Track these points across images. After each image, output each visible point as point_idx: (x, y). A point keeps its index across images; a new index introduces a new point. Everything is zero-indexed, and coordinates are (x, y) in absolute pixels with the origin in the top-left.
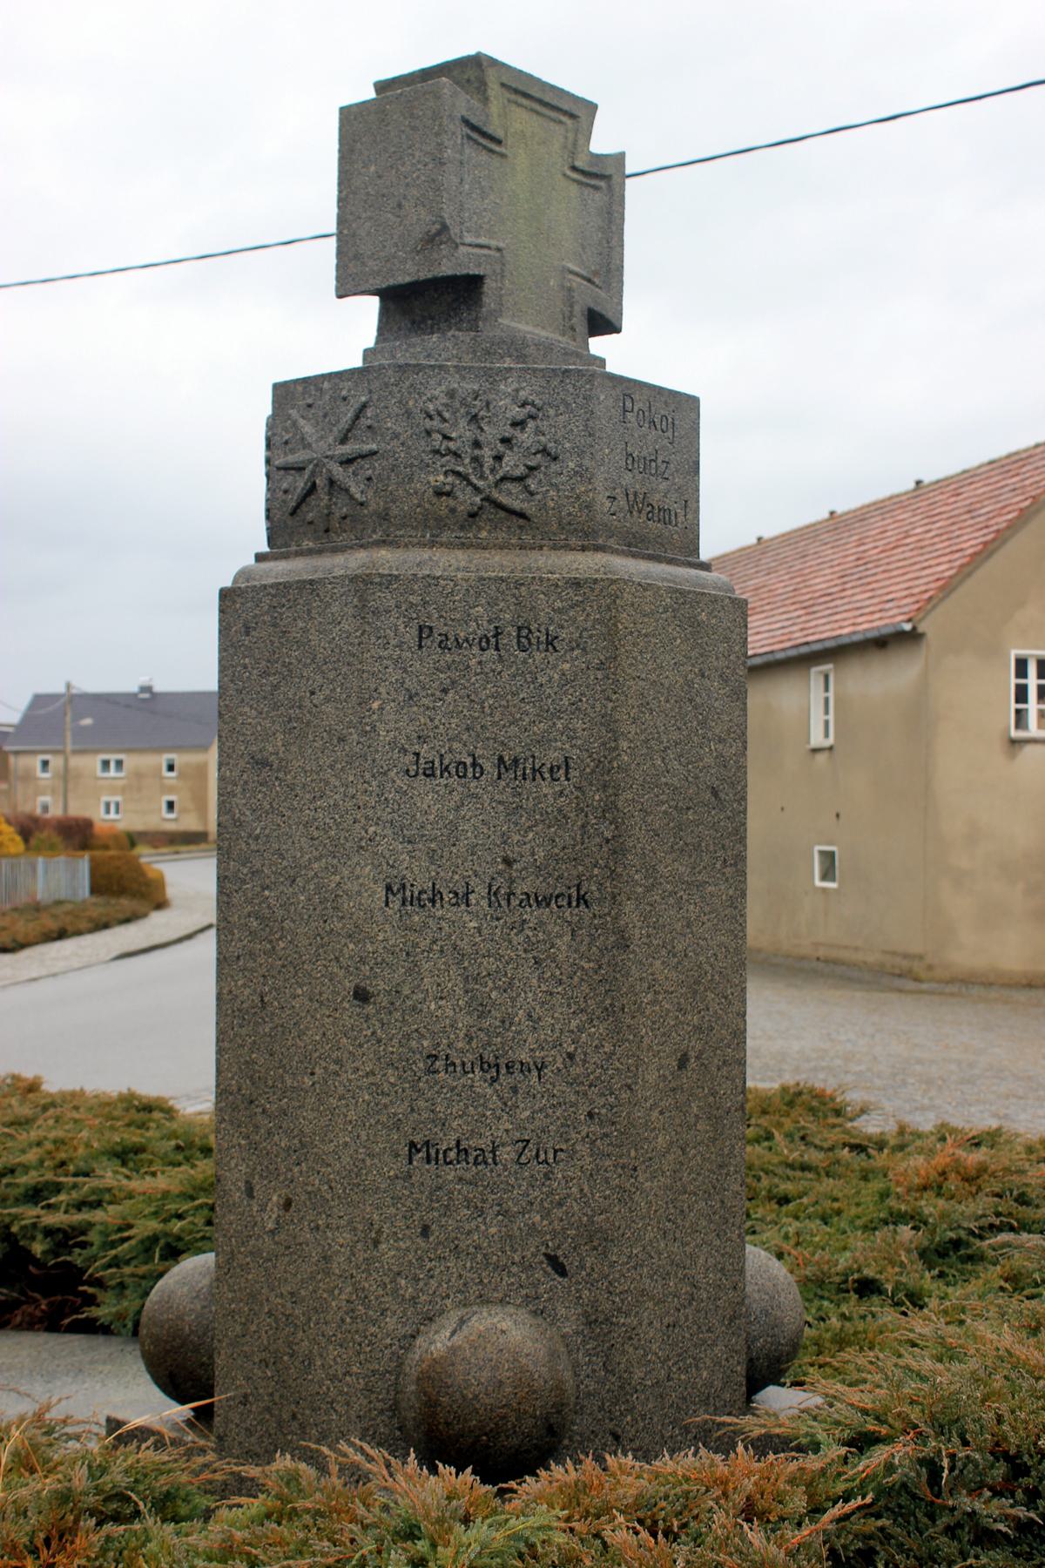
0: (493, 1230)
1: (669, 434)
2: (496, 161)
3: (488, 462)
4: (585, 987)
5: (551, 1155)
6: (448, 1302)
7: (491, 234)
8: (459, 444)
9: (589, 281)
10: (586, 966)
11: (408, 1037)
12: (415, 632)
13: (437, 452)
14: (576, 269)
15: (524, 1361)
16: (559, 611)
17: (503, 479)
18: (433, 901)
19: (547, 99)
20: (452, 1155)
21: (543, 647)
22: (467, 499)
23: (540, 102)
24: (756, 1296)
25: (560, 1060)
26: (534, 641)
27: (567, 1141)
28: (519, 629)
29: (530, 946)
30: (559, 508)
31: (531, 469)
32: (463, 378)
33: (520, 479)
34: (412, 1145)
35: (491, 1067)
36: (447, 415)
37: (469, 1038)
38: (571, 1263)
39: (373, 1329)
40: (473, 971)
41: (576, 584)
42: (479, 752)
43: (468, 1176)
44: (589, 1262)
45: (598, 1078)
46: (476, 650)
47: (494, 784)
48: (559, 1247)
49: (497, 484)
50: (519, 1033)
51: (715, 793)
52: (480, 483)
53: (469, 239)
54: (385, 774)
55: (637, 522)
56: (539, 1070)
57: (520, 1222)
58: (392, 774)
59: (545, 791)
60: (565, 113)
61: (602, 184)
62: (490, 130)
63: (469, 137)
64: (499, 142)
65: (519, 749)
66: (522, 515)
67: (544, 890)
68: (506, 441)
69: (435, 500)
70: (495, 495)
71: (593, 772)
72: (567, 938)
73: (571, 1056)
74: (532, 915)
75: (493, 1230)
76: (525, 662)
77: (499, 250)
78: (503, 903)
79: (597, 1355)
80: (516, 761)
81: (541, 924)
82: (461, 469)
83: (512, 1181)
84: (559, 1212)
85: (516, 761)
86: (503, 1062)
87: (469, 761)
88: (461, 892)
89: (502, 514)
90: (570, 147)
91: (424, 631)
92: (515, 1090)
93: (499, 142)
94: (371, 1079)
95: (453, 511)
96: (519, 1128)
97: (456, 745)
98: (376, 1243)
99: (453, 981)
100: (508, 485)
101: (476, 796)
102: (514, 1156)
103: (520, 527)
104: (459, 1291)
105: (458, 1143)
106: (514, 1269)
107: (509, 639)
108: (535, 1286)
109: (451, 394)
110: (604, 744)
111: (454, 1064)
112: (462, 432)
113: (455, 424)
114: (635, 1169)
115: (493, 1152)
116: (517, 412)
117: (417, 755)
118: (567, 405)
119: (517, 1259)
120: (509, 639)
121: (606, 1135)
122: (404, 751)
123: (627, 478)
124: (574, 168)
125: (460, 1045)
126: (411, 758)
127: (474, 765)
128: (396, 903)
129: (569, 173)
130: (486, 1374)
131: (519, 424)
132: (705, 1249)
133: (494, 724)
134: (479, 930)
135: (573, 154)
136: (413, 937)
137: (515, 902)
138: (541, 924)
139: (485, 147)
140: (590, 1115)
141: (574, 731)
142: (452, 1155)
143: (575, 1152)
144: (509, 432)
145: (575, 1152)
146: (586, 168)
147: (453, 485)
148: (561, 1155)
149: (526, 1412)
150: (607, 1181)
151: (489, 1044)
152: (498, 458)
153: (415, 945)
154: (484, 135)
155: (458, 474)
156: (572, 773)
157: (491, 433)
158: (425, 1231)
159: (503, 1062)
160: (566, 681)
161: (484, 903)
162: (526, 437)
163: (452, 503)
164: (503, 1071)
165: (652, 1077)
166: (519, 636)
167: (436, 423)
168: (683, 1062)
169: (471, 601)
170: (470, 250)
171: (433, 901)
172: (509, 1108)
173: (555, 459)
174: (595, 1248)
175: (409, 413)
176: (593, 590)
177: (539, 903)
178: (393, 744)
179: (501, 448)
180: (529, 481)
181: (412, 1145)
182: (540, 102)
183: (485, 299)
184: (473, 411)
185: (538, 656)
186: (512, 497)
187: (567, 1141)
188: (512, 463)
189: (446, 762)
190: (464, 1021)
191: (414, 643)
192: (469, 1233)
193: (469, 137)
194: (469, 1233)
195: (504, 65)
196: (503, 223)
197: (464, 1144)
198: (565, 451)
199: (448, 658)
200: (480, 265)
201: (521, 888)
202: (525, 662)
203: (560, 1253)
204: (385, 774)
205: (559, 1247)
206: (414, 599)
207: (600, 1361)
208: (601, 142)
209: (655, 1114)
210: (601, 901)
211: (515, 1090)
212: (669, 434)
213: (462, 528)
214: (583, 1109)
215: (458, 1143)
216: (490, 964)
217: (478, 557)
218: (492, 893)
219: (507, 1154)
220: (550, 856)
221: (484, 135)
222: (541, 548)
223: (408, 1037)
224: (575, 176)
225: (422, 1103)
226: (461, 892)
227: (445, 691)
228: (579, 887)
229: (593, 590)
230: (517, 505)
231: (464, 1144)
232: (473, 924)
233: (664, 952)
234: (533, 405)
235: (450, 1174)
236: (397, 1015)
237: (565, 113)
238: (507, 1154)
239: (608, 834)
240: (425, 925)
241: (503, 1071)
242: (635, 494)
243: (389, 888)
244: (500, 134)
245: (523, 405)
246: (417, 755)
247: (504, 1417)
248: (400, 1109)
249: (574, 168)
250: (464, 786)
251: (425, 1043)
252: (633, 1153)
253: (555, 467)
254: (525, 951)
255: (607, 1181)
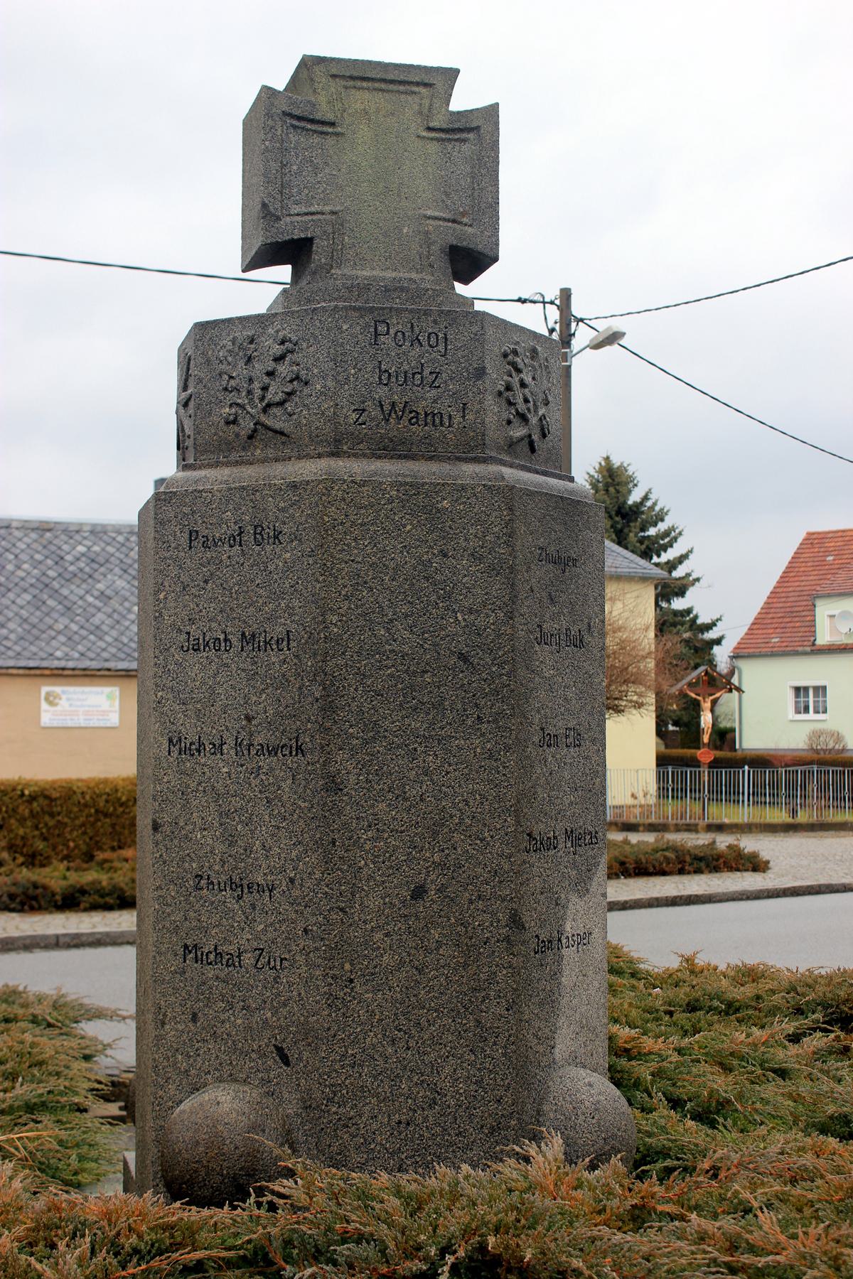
0: (239, 1021)
1: (441, 348)
2: (331, 141)
3: (258, 392)
4: (301, 823)
5: (278, 963)
6: (209, 1077)
7: (326, 201)
8: (237, 381)
9: (454, 221)
10: (303, 805)
11: (183, 860)
12: (187, 536)
13: (226, 389)
14: (437, 214)
15: (220, 1128)
16: (283, 510)
17: (269, 405)
18: (199, 751)
19: (390, 77)
20: (212, 957)
21: (271, 541)
22: (247, 425)
23: (384, 81)
24: (552, 1115)
25: (284, 883)
26: (265, 536)
27: (290, 951)
28: (256, 527)
29: (264, 788)
30: (309, 424)
31: (289, 394)
32: (244, 327)
33: (281, 404)
34: (186, 947)
35: (239, 886)
36: (230, 359)
37: (223, 862)
38: (293, 1055)
39: (161, 1093)
40: (225, 808)
41: (294, 486)
42: (229, 630)
43: (222, 975)
44: (306, 1055)
45: (311, 900)
46: (226, 547)
47: (238, 655)
48: (284, 1041)
49: (265, 410)
50: (256, 859)
51: (463, 657)
52: (253, 411)
53: (296, 209)
54: (167, 650)
55: (396, 428)
56: (271, 891)
57: (256, 1018)
58: (172, 650)
59: (274, 659)
60: (418, 84)
61: (471, 136)
62: (318, 116)
63: (295, 127)
64: (332, 124)
65: (255, 626)
66: (282, 433)
67: (274, 741)
68: (270, 374)
69: (225, 428)
70: (263, 418)
71: (307, 642)
72: (289, 782)
73: (292, 880)
74: (265, 762)
75: (239, 1021)
76: (259, 554)
77: (333, 213)
78: (246, 752)
79: (312, 1136)
80: (253, 636)
81: (271, 769)
82: (239, 401)
83: (252, 982)
84: (284, 1011)
85: (253, 636)
86: (245, 882)
87: (222, 637)
88: (217, 743)
89: (270, 434)
90: (425, 111)
91: (193, 535)
92: (253, 907)
93: (332, 124)
94: (160, 892)
95: (237, 435)
96: (257, 938)
97: (214, 625)
98: (163, 1024)
99: (213, 818)
100: (275, 410)
101: (227, 665)
102: (253, 961)
103: (283, 443)
104: (216, 1069)
105: (216, 949)
106: (254, 1056)
107: (248, 538)
108: (268, 1070)
109: (234, 341)
110: (314, 618)
111: (212, 883)
112: (240, 370)
113: (235, 366)
114: (351, 981)
115: (239, 956)
116: (277, 349)
117: (188, 633)
118: (316, 338)
119: (255, 1047)
120: (248, 538)
121: (317, 949)
122: (180, 631)
123: (382, 392)
124: (429, 129)
125: (217, 868)
126: (184, 636)
127: (226, 640)
128: (175, 750)
129: (424, 134)
130: (190, 1134)
131: (279, 359)
132: (451, 1060)
133: (239, 606)
134: (229, 773)
135: (429, 117)
136: (186, 779)
137: (253, 752)
138: (271, 769)
139: (315, 132)
140: (306, 931)
141: (293, 608)
142: (212, 957)
143: (295, 962)
144: (271, 365)
145: (295, 962)
146: (444, 126)
147: (236, 414)
148: (286, 964)
149: (213, 1170)
150: (317, 987)
151: (236, 868)
152: (265, 389)
153: (188, 786)
154: (312, 121)
155: (238, 405)
156: (293, 644)
157: (259, 368)
158: (194, 1018)
159: (245, 882)
160: (288, 568)
161: (233, 752)
162: (283, 369)
163: (236, 429)
164: (246, 891)
165: (374, 902)
166: (255, 533)
167: (223, 367)
168: (419, 893)
169: (223, 507)
170: (299, 218)
171: (199, 751)
172: (250, 921)
173: (306, 383)
174: (309, 1045)
175: (208, 361)
176: (305, 490)
177: (270, 753)
178: (173, 625)
179: (266, 380)
180: (287, 405)
181: (186, 947)
182: (384, 81)
183: (315, 257)
184: (249, 353)
185: (269, 548)
186: (276, 420)
187: (290, 951)
188: (275, 394)
189: (207, 639)
190: (220, 848)
191: (186, 545)
192: (223, 1022)
193: (295, 127)
194: (223, 1022)
195: (333, 59)
196: (376, 189)
197: (220, 949)
198: (314, 375)
199: (208, 555)
200: (307, 229)
201: (258, 739)
202: (259, 554)
203: (285, 1046)
204: (167, 650)
205: (284, 1041)
206: (186, 510)
207: (313, 1140)
208: (462, 99)
209: (378, 936)
210: (312, 751)
211: (253, 907)
212: (441, 348)
213: (244, 449)
214: (301, 925)
215: (216, 949)
216: (237, 803)
217: (236, 471)
218: (238, 744)
219: (248, 959)
220: (277, 713)
221: (312, 121)
222: (290, 458)
223: (183, 860)
224: (433, 135)
225: (192, 914)
226: (217, 743)
227: (206, 582)
228: (297, 739)
229: (305, 490)
230: (278, 425)
231: (220, 949)
232: (225, 770)
233: (390, 796)
234: (290, 341)
235: (210, 972)
236: (176, 842)
237: (418, 84)
238: (248, 959)
239: (317, 695)
240: (194, 770)
241: (246, 891)
242: (393, 405)
243: (170, 741)
244: (330, 117)
245: (282, 343)
246: (188, 633)
247: (196, 1171)
248: (178, 917)
249: (429, 129)
250: (218, 657)
251: (194, 865)
252: (347, 967)
253: (306, 391)
254: (260, 792)
255: (317, 987)
